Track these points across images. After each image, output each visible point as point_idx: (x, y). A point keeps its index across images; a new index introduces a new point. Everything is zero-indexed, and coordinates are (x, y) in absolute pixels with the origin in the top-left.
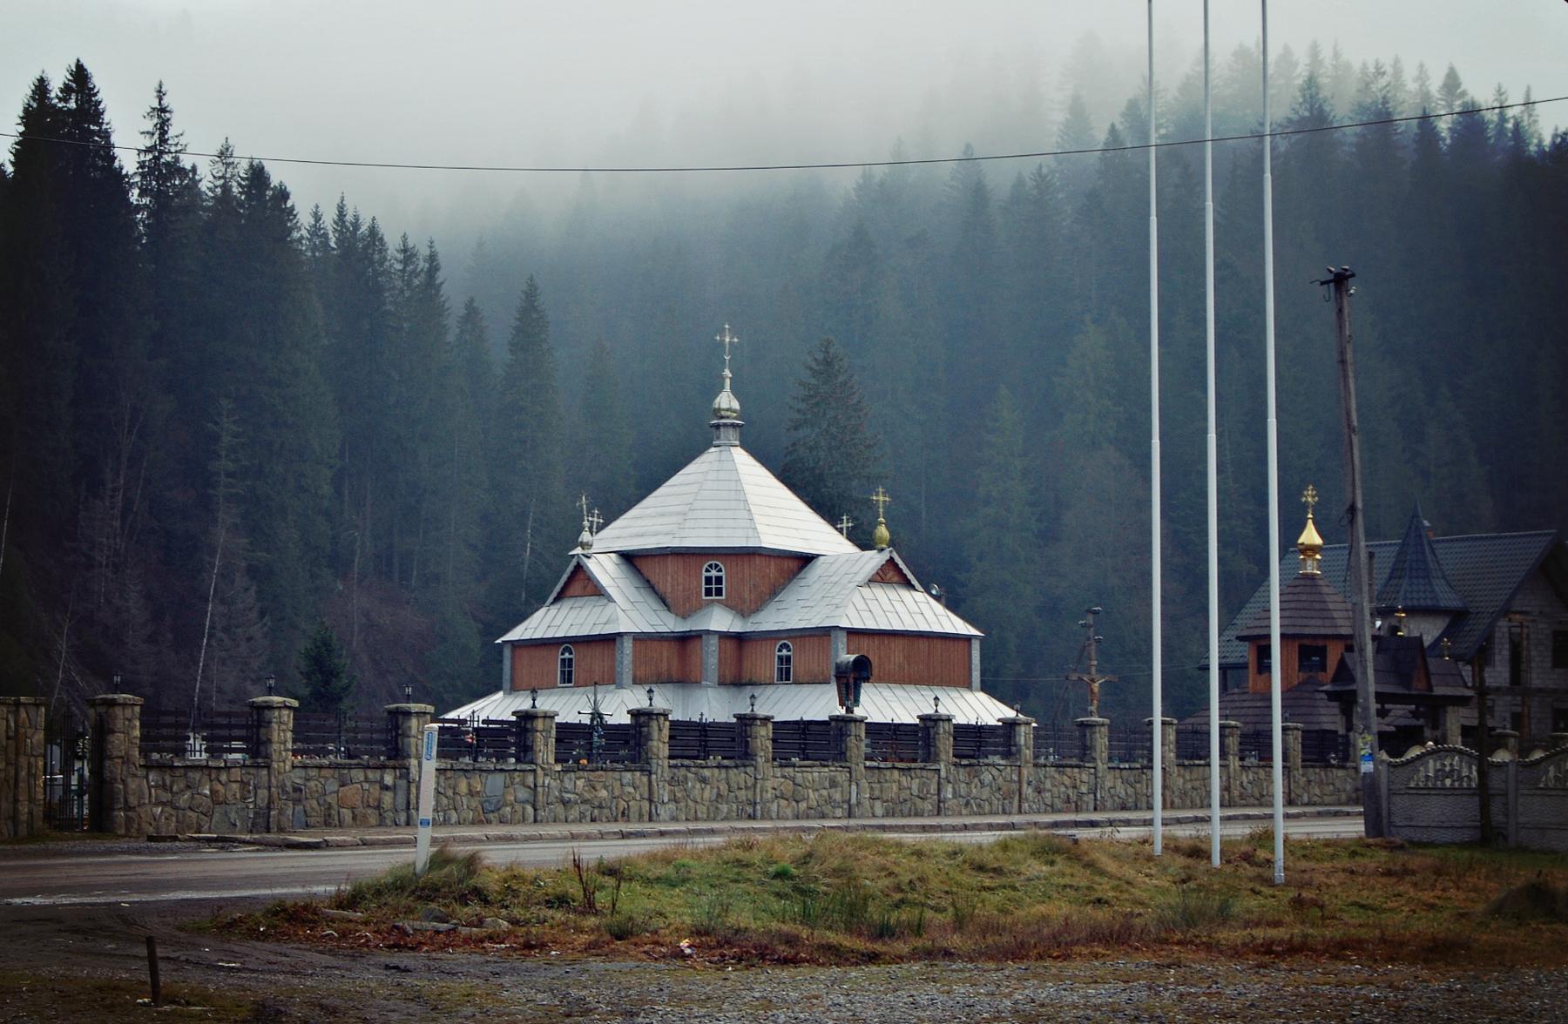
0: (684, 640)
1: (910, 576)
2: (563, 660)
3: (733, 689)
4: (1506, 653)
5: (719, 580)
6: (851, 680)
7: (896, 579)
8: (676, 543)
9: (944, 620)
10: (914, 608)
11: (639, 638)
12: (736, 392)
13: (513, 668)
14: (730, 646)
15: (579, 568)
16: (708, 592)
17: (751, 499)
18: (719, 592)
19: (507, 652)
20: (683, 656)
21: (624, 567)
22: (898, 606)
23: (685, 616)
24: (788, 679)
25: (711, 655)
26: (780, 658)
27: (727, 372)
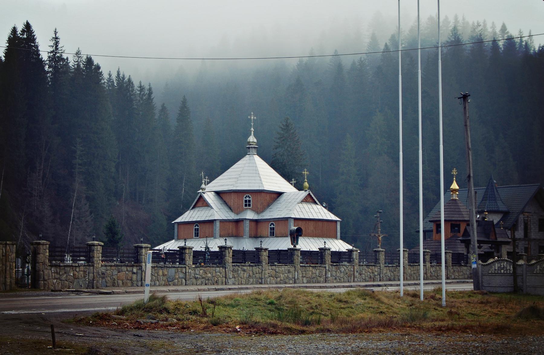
0: (237, 222)
1: (316, 200)
2: (195, 229)
3: (254, 239)
4: (522, 226)
5: (249, 201)
6: (295, 236)
7: (311, 201)
8: (234, 188)
9: (328, 215)
10: (317, 211)
11: (222, 221)
12: (255, 136)
13: (178, 232)
14: (253, 224)
15: (201, 197)
16: (246, 205)
17: (260, 173)
18: (249, 205)
19: (176, 226)
20: (237, 228)
21: (216, 197)
22: (312, 210)
23: (238, 214)
24: (273, 235)
25: (247, 227)
26: (271, 228)
27: (252, 129)
